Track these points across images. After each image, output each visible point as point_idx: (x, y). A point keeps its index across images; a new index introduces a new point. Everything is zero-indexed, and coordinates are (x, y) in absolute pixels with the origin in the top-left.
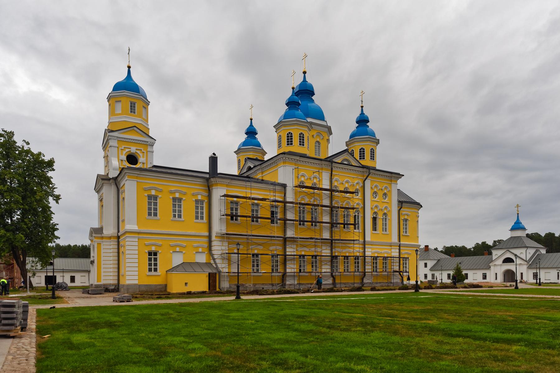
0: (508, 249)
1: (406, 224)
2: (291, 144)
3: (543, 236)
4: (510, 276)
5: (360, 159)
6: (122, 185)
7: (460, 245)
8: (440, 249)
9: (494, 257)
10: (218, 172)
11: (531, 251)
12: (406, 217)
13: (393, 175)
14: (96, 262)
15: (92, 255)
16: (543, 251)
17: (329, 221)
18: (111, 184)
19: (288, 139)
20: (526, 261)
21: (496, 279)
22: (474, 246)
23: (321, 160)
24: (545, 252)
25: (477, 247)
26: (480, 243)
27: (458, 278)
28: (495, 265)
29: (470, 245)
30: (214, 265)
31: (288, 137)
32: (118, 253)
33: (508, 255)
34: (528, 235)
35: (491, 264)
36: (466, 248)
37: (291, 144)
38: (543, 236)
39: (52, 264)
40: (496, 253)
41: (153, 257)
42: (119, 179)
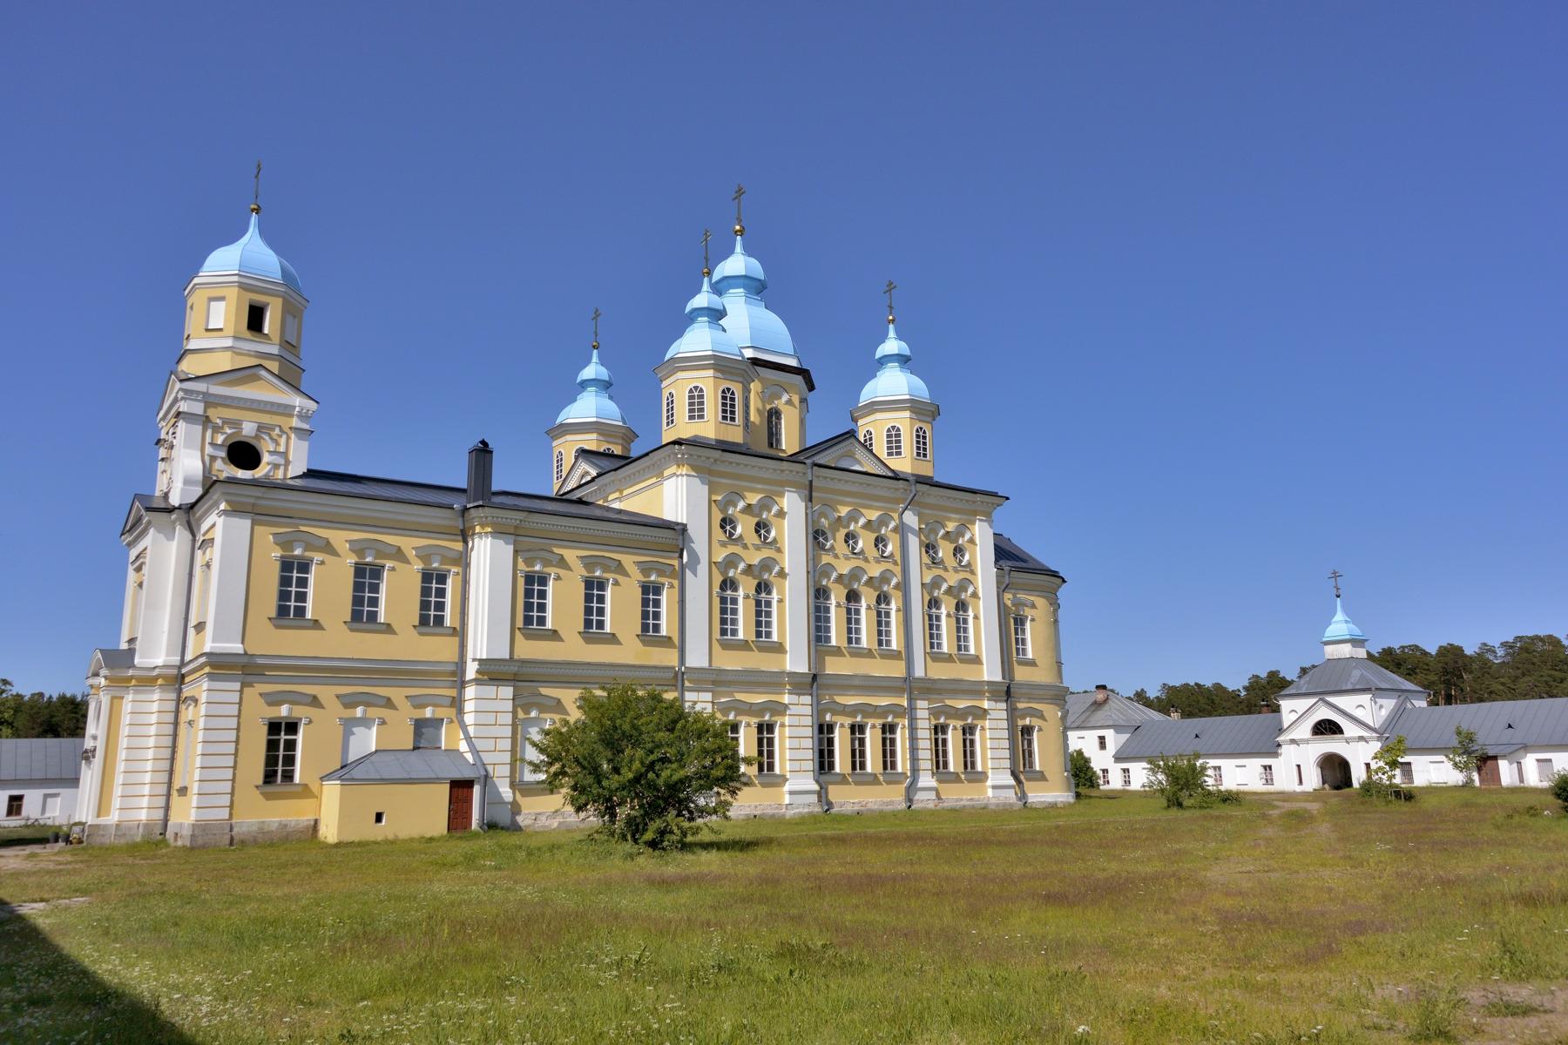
0: (1321, 694)
2: (701, 417)
3: (1434, 653)
5: (890, 454)
6: (205, 526)
8: (1153, 693)
9: (1287, 718)
10: (495, 488)
11: (1389, 704)
12: (1027, 721)
13: (978, 498)
14: (99, 754)
15: (91, 728)
17: (465, 486)
18: (174, 522)
19: (691, 404)
21: (1301, 782)
23: (781, 459)
24: (1424, 704)
25: (1255, 685)
26: (1263, 675)
27: (1183, 784)
28: (1293, 741)
29: (1236, 682)
30: (469, 757)
31: (691, 397)
32: (176, 724)
33: (1324, 713)
37: (701, 417)
38: (1434, 653)
39: (547, 733)
40: (1290, 708)
41: (283, 737)
42: (199, 511)
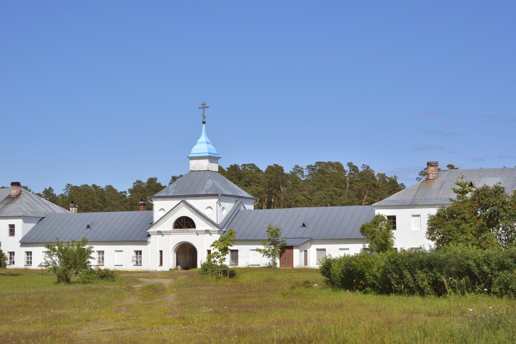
0: (183, 197)
1: (31, 258)
3: (264, 171)
4: (186, 253)
7: (102, 185)
9: (157, 214)
16: (250, 207)
20: (216, 225)
21: (161, 264)
22: (131, 187)
27: (73, 263)
28: (159, 233)
29: (124, 186)
34: (221, 170)
35: (150, 231)
36: (115, 191)
38: (264, 171)
40: (160, 207)
